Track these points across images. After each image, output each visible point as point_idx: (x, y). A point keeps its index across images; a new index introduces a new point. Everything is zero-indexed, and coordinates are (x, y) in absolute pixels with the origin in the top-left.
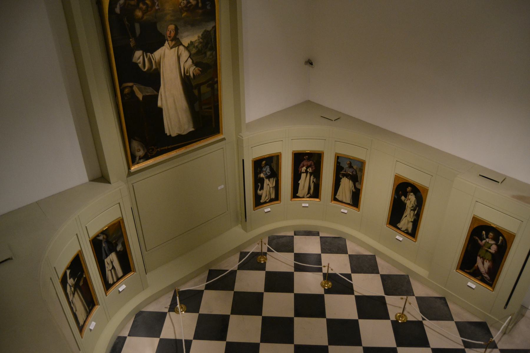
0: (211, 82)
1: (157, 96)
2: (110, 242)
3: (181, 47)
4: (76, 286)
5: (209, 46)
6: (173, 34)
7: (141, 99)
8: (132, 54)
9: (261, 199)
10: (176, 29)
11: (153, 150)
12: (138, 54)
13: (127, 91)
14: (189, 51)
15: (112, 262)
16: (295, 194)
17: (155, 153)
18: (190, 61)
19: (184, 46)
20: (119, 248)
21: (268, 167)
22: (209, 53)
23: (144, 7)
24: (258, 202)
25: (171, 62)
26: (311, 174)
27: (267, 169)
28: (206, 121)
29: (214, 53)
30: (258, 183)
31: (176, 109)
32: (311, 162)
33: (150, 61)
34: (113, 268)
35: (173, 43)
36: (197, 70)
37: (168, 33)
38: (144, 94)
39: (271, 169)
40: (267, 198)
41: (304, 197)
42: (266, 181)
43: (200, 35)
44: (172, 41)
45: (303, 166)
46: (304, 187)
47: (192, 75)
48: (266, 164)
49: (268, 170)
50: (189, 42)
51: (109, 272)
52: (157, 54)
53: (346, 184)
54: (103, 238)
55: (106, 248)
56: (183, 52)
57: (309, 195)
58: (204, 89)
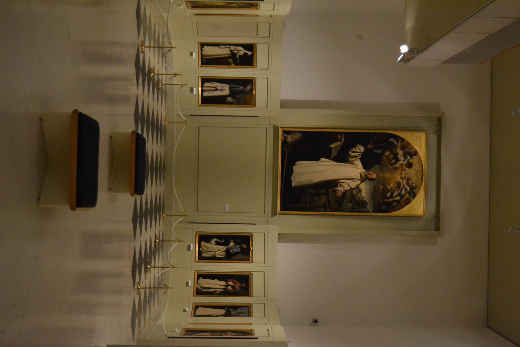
1: (328, 158)
2: (242, 93)
3: (359, 182)
4: (233, 55)
5: (355, 206)
6: (370, 176)
7: (331, 146)
8: (363, 145)
10: (372, 180)
12: (362, 149)
13: (339, 137)
14: (355, 188)
15: (221, 90)
16: (201, 276)
17: (285, 150)
18: (348, 188)
19: (360, 184)
20: (230, 99)
21: (239, 250)
22: (350, 205)
23: (390, 158)
24: (204, 238)
25: (349, 173)
27: (237, 249)
28: (296, 199)
29: (349, 210)
30: (224, 239)
31: (315, 172)
32: (239, 289)
33: (355, 157)
34: (217, 90)
35: (364, 176)
36: (340, 194)
37: (371, 173)
38: (333, 149)
39: (236, 254)
40: (204, 248)
42: (223, 248)
44: (366, 175)
45: (234, 283)
47: (337, 189)
48: (242, 249)
49: (235, 250)
50: (362, 189)
52: (358, 163)
55: (237, 89)
58: (323, 199)
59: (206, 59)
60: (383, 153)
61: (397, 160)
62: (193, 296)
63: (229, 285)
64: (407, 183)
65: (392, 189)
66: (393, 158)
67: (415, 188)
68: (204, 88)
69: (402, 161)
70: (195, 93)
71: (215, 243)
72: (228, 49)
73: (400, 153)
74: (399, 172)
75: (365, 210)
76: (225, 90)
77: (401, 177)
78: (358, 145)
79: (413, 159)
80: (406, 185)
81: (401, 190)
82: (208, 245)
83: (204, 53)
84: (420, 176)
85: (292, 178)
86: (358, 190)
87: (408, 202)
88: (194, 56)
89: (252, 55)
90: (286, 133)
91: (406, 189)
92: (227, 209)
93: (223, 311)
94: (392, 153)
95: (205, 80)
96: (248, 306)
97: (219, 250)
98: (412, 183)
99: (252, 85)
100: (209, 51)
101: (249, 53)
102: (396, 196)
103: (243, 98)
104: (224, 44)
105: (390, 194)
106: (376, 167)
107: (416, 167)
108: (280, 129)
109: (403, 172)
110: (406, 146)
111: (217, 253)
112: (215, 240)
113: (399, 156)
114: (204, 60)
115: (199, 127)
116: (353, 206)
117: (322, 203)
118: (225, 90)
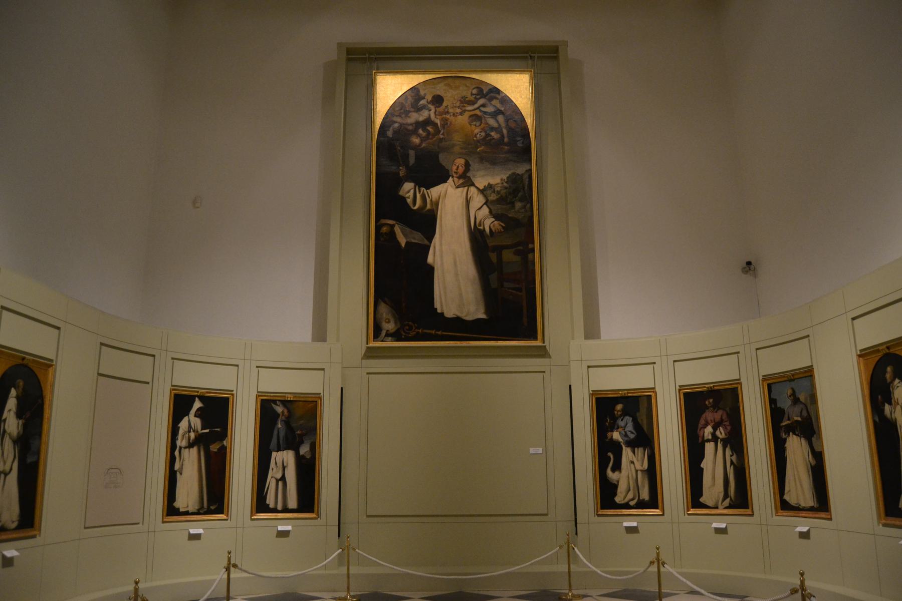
0: (521, 248)
1: (428, 248)
2: (289, 423)
3: (472, 189)
4: (199, 441)
5: (520, 194)
6: (461, 170)
7: (403, 245)
9: (615, 494)
10: (467, 166)
11: (411, 328)
13: (384, 229)
14: (485, 196)
15: (284, 468)
16: (695, 498)
17: (412, 334)
18: (485, 210)
20: (304, 450)
21: (628, 419)
22: (518, 205)
23: (424, 134)
24: (607, 496)
25: (457, 209)
26: (725, 443)
27: (627, 423)
28: (511, 311)
29: (528, 206)
30: (607, 454)
31: (456, 275)
32: (720, 412)
33: (424, 198)
34: (283, 478)
37: (454, 168)
40: (630, 496)
41: (717, 508)
42: (627, 454)
43: (505, 178)
44: (459, 178)
46: (714, 478)
47: (487, 230)
49: (630, 427)
50: (486, 184)
51: (273, 483)
53: (796, 446)
54: (283, 412)
55: (282, 434)
56: (475, 196)
57: (727, 501)
59: (209, 504)
60: (416, 148)
61: (428, 122)
62: (752, 515)
63: (714, 434)
64: (472, 103)
65: (483, 130)
66: (424, 130)
67: (480, 90)
68: (279, 507)
69: (430, 113)
70: (289, 528)
71: (617, 473)
72: (185, 452)
73: (414, 117)
74: (452, 118)
75: (526, 176)
76: (284, 460)
77: (461, 114)
78: (401, 193)
79: (425, 94)
80: (476, 106)
81: (485, 113)
82: (622, 488)
83: (193, 506)
84: (457, 82)
85: (469, 318)
86: (489, 192)
87: (506, 100)
88: (201, 531)
89: (202, 398)
90: (377, 332)
91: (483, 106)
92: (540, 451)
93: (796, 446)
94: (415, 132)
95: (261, 505)
96: (769, 386)
97: (632, 462)
98: (472, 94)
99: (274, 402)
100: (189, 492)
101: (197, 404)
102: (498, 122)
103: (302, 422)
104: (172, 460)
105: (493, 134)
106: (442, 158)
107: (440, 90)
108: (372, 344)
109: (451, 110)
110: (399, 107)
111: (638, 467)
112: (609, 473)
113: (421, 119)
114: (212, 508)
115: (368, 516)
116: (521, 200)
117: (517, 259)
118: (284, 460)
